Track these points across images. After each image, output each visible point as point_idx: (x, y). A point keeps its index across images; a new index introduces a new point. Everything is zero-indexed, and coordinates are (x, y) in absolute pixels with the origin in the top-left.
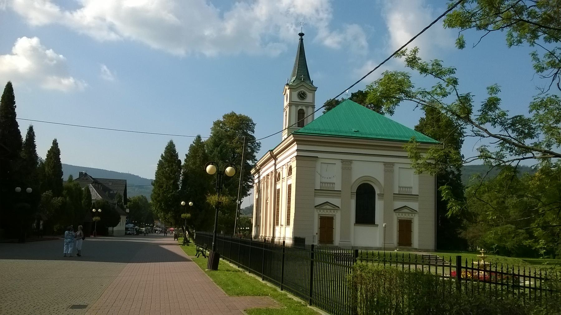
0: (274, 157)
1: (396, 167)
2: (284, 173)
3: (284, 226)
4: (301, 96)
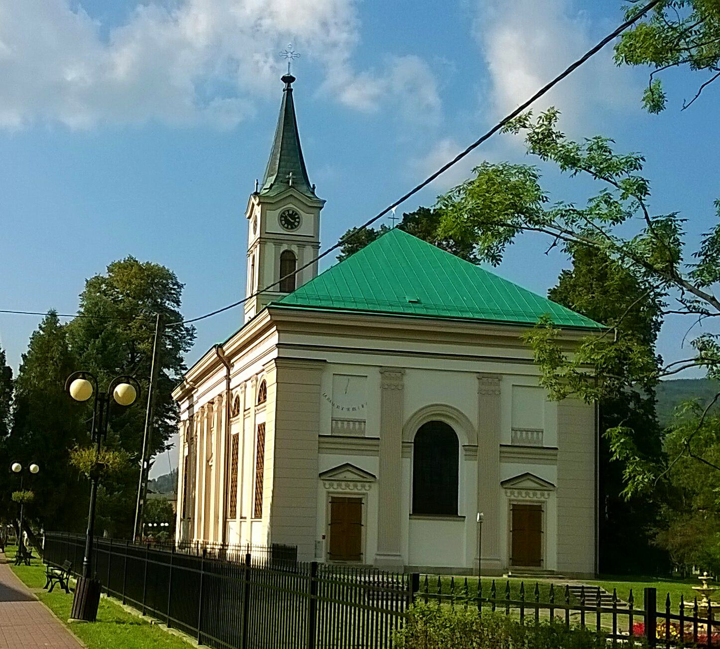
0: (226, 361)
1: (506, 385)
2: (249, 397)
3: (249, 520)
4: (287, 222)
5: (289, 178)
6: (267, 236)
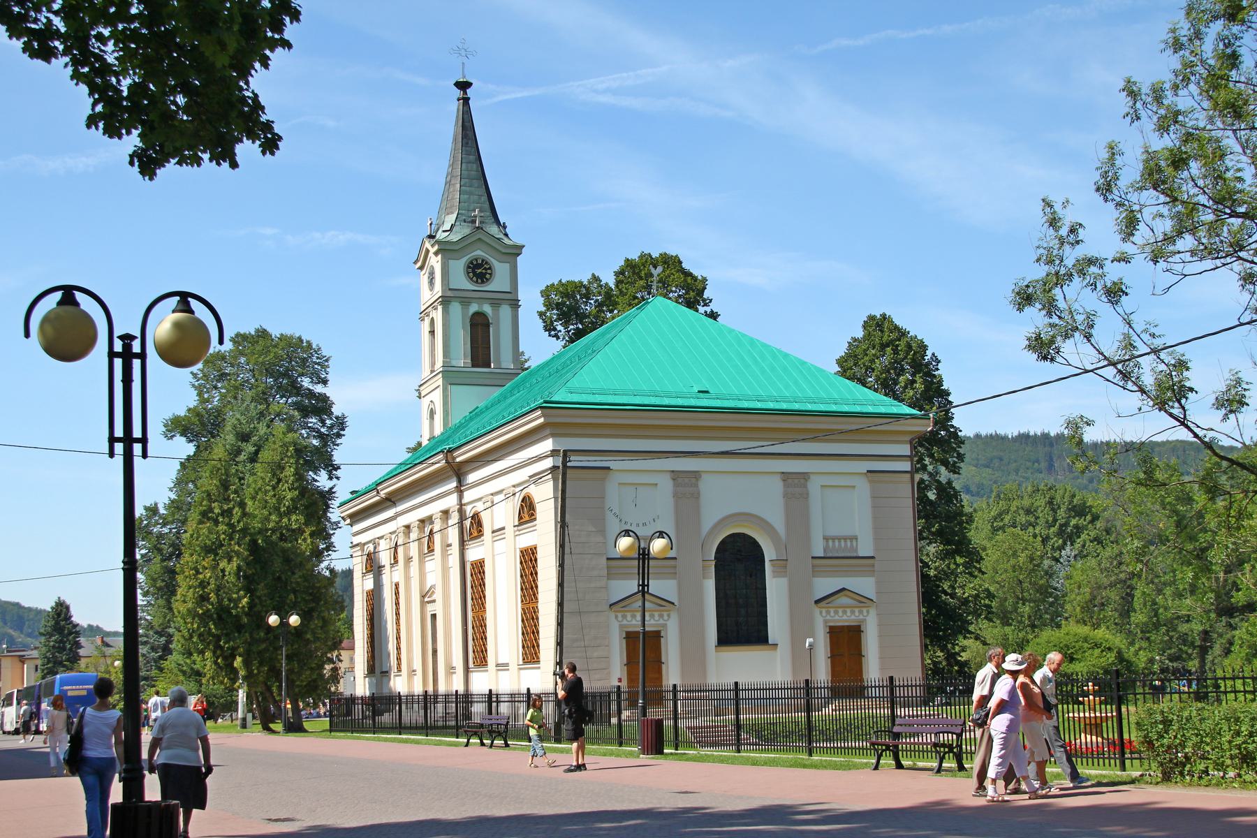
0: (458, 472)
1: (814, 486)
6: (449, 294)
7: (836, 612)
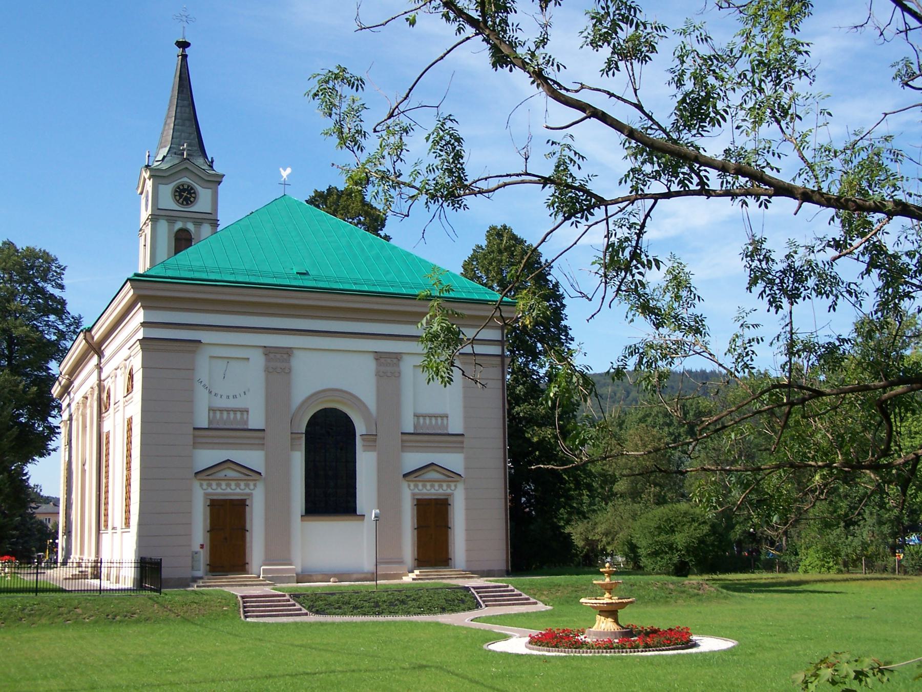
2: (117, 387)
3: (119, 531)
5: (184, 150)
7: (424, 486)
